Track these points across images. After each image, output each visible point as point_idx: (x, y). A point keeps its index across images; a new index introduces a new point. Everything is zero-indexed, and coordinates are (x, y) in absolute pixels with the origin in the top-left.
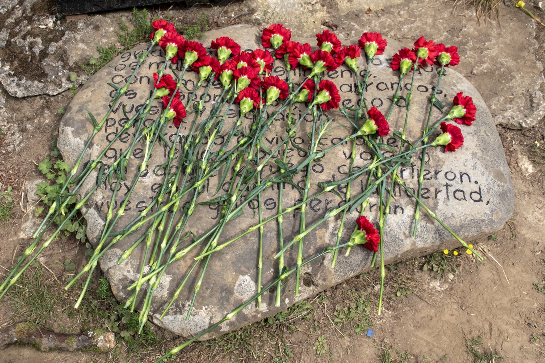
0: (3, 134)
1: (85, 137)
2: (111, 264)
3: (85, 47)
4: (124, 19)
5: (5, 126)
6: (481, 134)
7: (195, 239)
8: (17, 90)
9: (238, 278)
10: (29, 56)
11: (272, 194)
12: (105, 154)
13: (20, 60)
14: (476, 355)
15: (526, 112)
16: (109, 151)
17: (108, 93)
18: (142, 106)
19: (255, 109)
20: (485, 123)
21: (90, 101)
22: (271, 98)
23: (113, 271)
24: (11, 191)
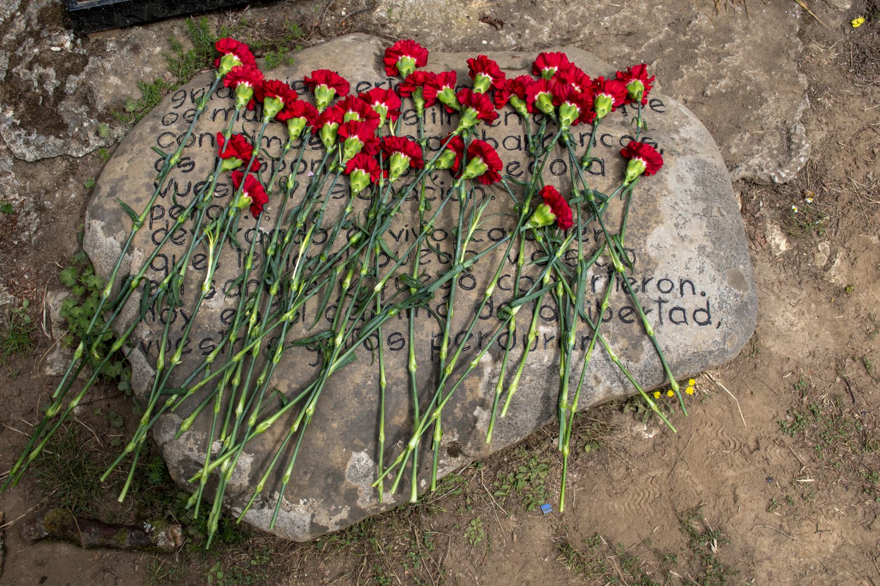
0: (14, 213)
1: (121, 236)
2: (167, 437)
3: (120, 83)
4: (176, 31)
5: (17, 200)
6: (713, 214)
7: (285, 402)
8: (25, 151)
9: (350, 456)
10: (39, 96)
11: (399, 326)
12: (151, 264)
13: (27, 102)
14: (693, 535)
15: (781, 158)
16: (158, 259)
17: (153, 165)
18: (203, 183)
19: (372, 185)
20: (719, 195)
21: (127, 177)
22: (396, 172)
23: (169, 449)
24: (29, 307)
